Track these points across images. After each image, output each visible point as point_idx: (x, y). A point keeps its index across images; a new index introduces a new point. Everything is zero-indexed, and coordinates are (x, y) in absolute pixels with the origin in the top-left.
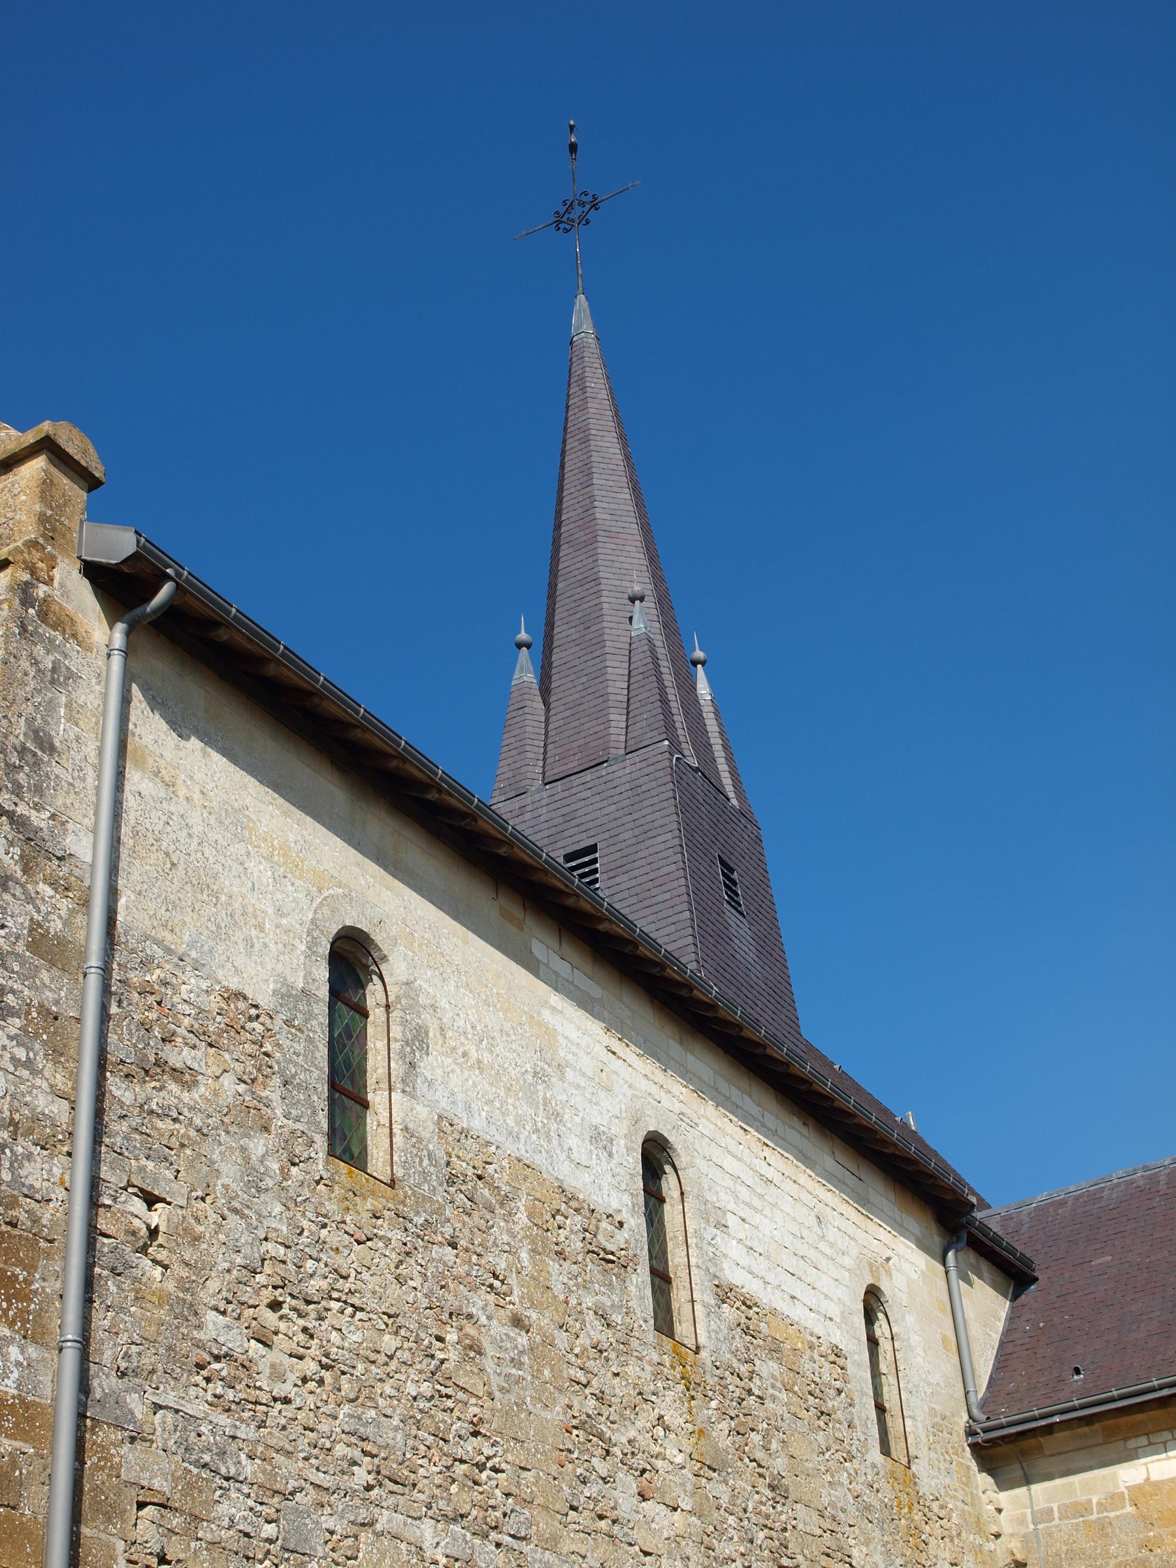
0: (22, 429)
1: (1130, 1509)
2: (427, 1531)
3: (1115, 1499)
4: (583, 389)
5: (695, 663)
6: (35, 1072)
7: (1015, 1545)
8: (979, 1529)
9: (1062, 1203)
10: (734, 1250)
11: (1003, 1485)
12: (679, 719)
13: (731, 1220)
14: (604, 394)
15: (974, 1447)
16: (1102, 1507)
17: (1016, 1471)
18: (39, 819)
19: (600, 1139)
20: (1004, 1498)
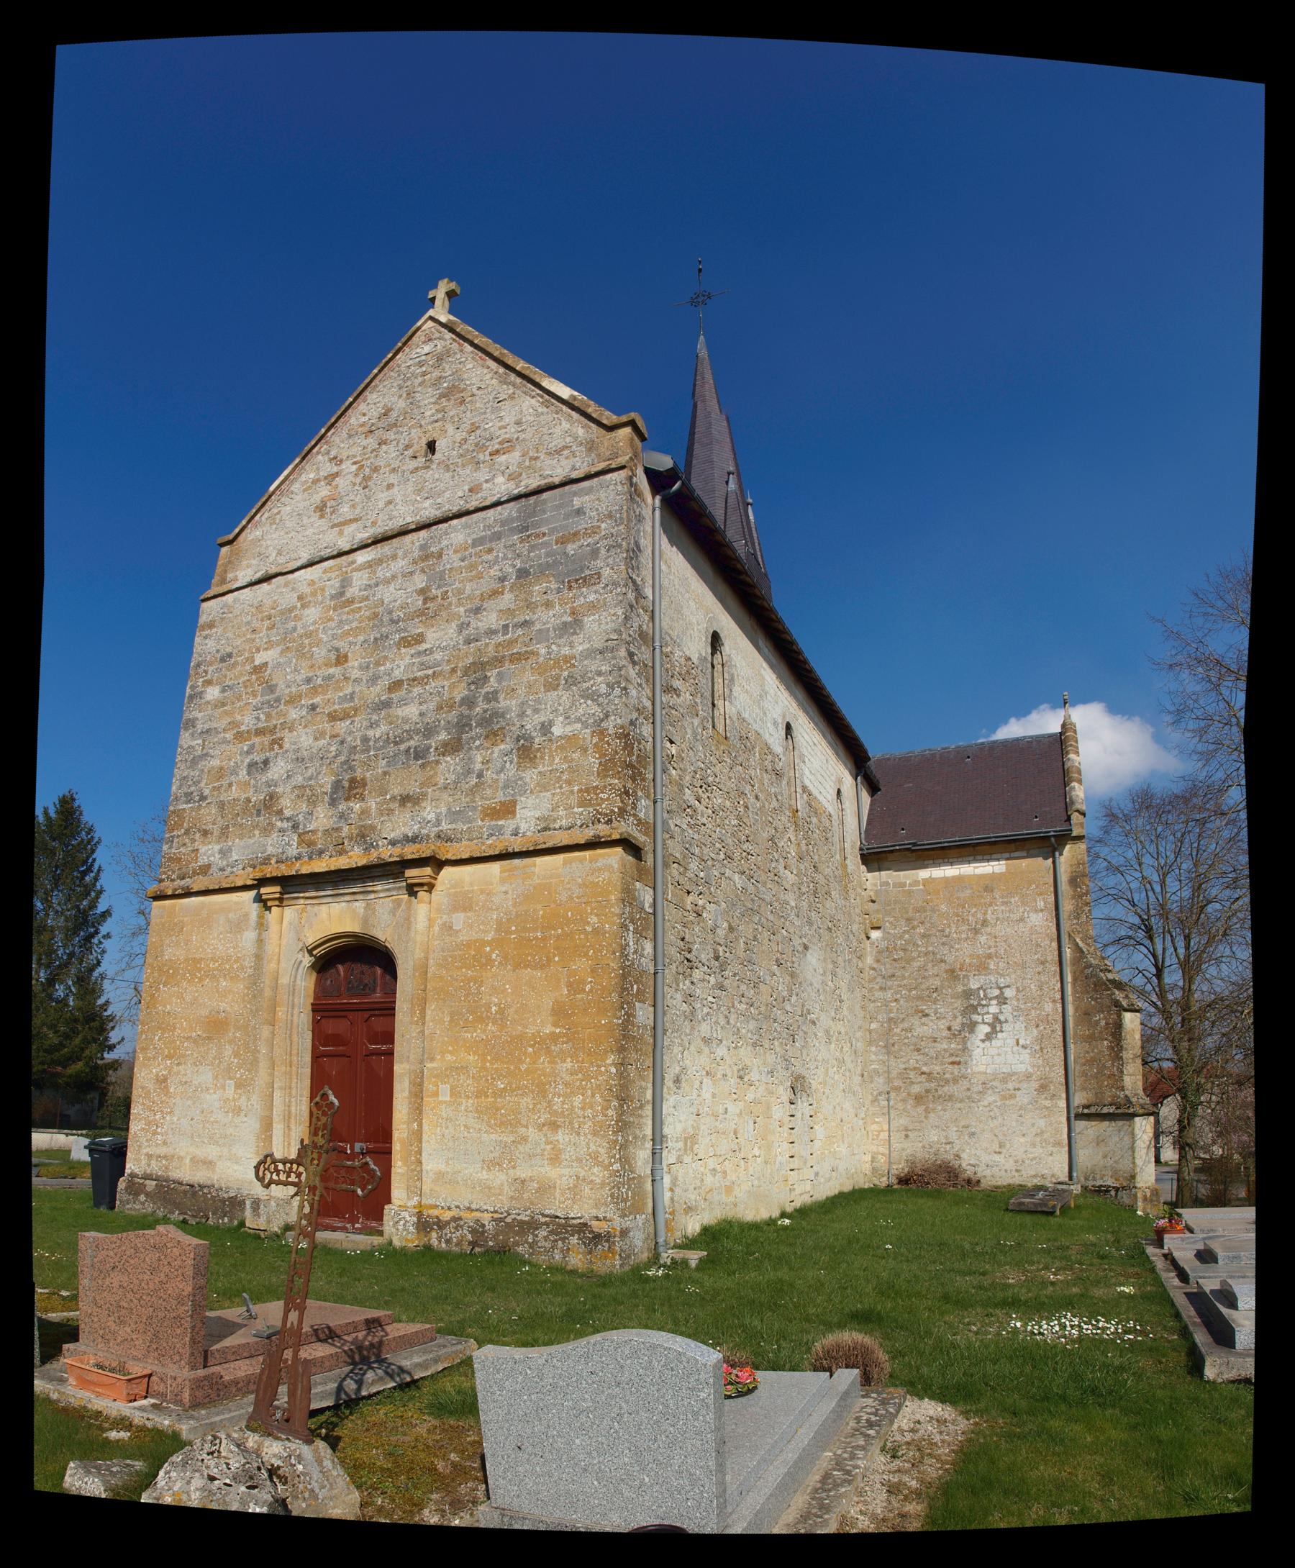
0: (618, 414)
1: (921, 887)
2: (736, 877)
3: (916, 883)
4: (703, 378)
5: (748, 504)
6: (643, 689)
7: (872, 893)
8: (861, 887)
9: (889, 759)
10: (807, 772)
11: (869, 871)
12: (747, 533)
13: (806, 760)
14: (711, 381)
15: (862, 855)
16: (910, 885)
17: (876, 865)
18: (639, 582)
19: (775, 723)
20: (869, 875)
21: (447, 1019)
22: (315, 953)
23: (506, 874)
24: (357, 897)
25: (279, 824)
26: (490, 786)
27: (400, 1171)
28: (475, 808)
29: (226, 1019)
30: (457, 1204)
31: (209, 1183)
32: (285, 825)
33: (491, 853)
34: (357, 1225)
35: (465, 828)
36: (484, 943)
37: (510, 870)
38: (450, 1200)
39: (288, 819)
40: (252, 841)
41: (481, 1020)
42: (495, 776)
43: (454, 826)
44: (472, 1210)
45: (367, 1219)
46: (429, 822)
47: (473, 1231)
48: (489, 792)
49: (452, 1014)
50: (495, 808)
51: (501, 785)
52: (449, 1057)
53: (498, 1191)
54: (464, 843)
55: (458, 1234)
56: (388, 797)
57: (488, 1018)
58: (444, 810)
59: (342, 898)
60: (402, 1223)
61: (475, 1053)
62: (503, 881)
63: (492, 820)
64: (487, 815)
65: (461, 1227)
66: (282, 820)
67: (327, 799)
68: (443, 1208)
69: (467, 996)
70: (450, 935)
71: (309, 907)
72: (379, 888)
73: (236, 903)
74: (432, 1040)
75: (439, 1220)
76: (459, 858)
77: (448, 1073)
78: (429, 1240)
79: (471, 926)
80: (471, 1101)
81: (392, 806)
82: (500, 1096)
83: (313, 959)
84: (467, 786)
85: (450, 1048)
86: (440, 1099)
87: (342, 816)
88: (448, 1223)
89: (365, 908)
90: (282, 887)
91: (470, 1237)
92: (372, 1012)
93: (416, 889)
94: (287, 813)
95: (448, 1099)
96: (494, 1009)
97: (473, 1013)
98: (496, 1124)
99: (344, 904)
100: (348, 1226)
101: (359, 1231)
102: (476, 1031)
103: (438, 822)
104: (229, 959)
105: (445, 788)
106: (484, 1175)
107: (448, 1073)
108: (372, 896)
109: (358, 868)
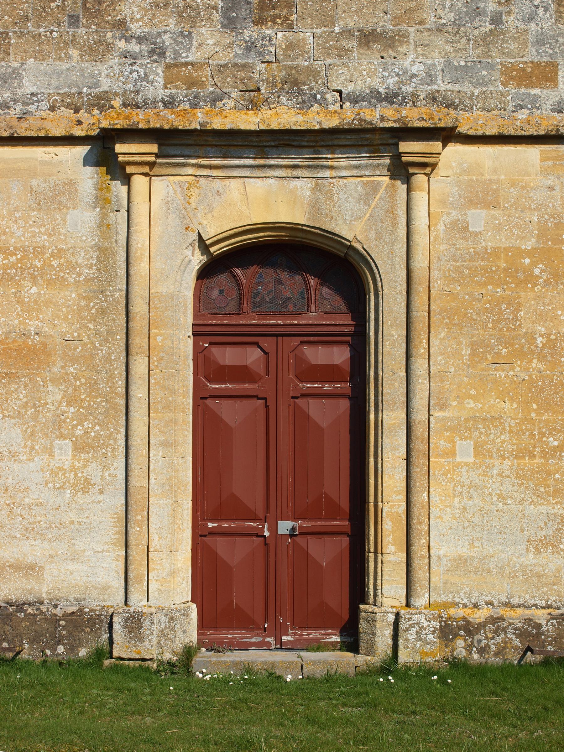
21: (466, 351)
22: (212, 249)
23: (551, 163)
24: (298, 173)
25: (122, 44)
26: (514, 38)
27: (392, 558)
28: (491, 67)
29: (45, 345)
30: (487, 599)
31: (31, 598)
32: (135, 47)
33: (533, 131)
34: (285, 638)
35: (476, 92)
36: (521, 253)
37: (556, 159)
38: (477, 594)
39: (140, 39)
40: (64, 66)
41: (521, 354)
42: (520, 25)
43: (457, 87)
44: (513, 607)
45: (301, 628)
46: (414, 76)
47: (522, 634)
48: (512, 46)
49: (473, 345)
50: (524, 70)
51: (531, 38)
52: (471, 404)
53: (551, 579)
54: (476, 113)
55: (498, 639)
56: (337, 29)
57: (532, 352)
58: (438, 61)
59: (270, 173)
60: (413, 630)
61: (512, 400)
62: (545, 172)
63: (519, 86)
64: (512, 78)
65: (504, 629)
66: (127, 40)
67: (216, 16)
68: (465, 606)
69: (496, 322)
70: (466, 239)
71: (202, 181)
72: (342, 163)
73: (44, 163)
74: (442, 381)
75: (468, 623)
76: (480, 133)
77: (470, 424)
78: (452, 651)
79: (499, 229)
80: (507, 463)
81: (344, 43)
82: (553, 456)
83: (205, 258)
84: (476, 32)
85: (473, 392)
86: (458, 459)
87: (250, 46)
88: (482, 626)
89: (312, 190)
90: (160, 146)
91: (517, 642)
92: (305, 339)
93: (411, 170)
94: (136, 28)
95: (471, 459)
96: (539, 341)
97: (507, 344)
98: (547, 493)
99: (271, 181)
100: (271, 640)
101: (292, 647)
102: (513, 369)
103: (430, 79)
104: (39, 251)
105: (439, 30)
106: (530, 559)
107: (470, 424)
108: (327, 173)
109: (323, 132)
